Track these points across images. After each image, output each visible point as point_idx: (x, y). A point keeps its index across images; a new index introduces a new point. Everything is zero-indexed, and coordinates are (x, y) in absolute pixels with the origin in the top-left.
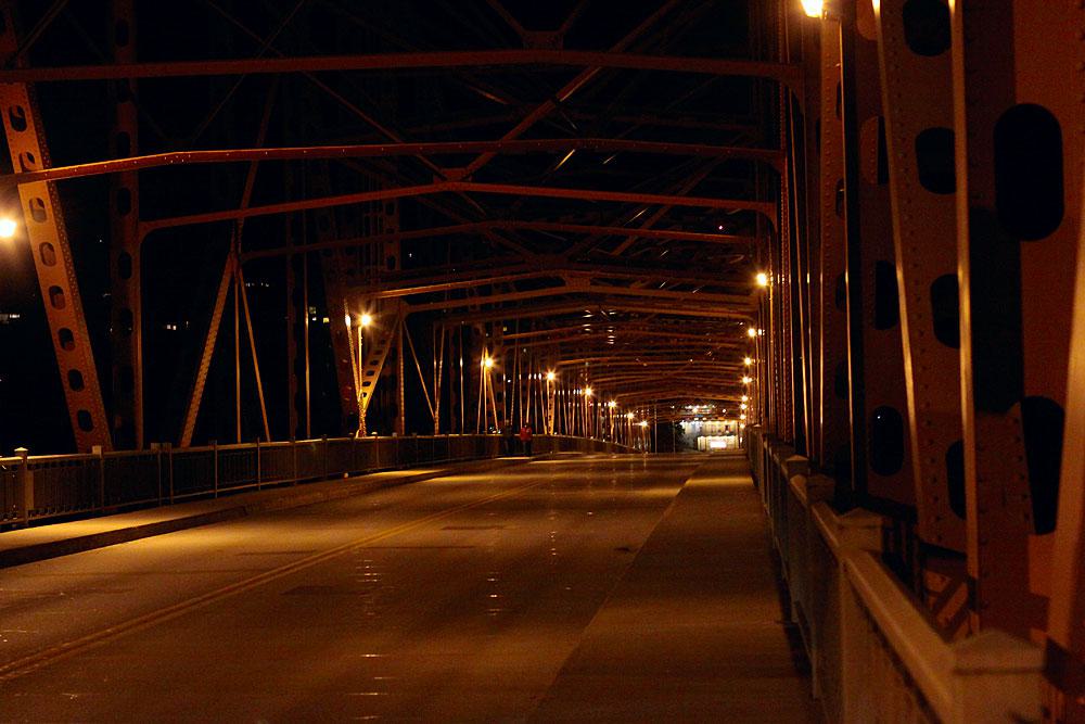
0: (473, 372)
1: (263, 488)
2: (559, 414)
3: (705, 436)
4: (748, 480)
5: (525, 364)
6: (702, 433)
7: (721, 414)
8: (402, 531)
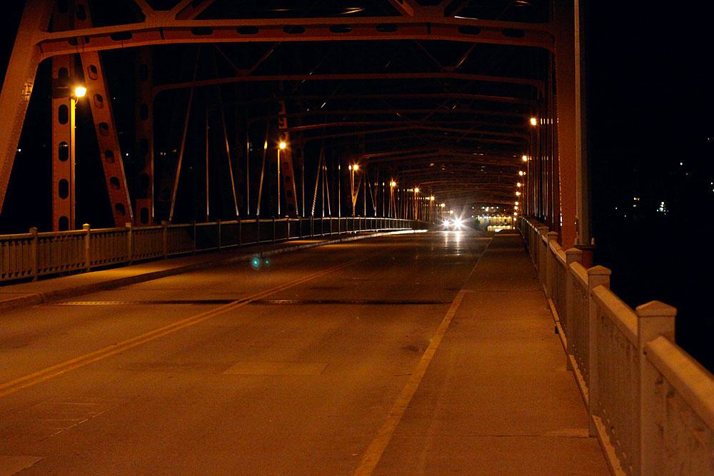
0: (388, 187)
1: (277, 242)
2: (420, 210)
3: (492, 226)
4: (518, 235)
5: (406, 184)
6: (491, 224)
7: (503, 212)
8: (322, 274)
